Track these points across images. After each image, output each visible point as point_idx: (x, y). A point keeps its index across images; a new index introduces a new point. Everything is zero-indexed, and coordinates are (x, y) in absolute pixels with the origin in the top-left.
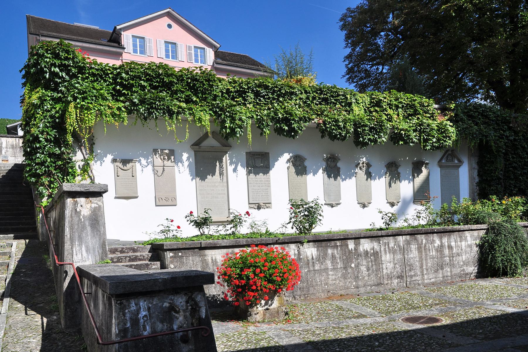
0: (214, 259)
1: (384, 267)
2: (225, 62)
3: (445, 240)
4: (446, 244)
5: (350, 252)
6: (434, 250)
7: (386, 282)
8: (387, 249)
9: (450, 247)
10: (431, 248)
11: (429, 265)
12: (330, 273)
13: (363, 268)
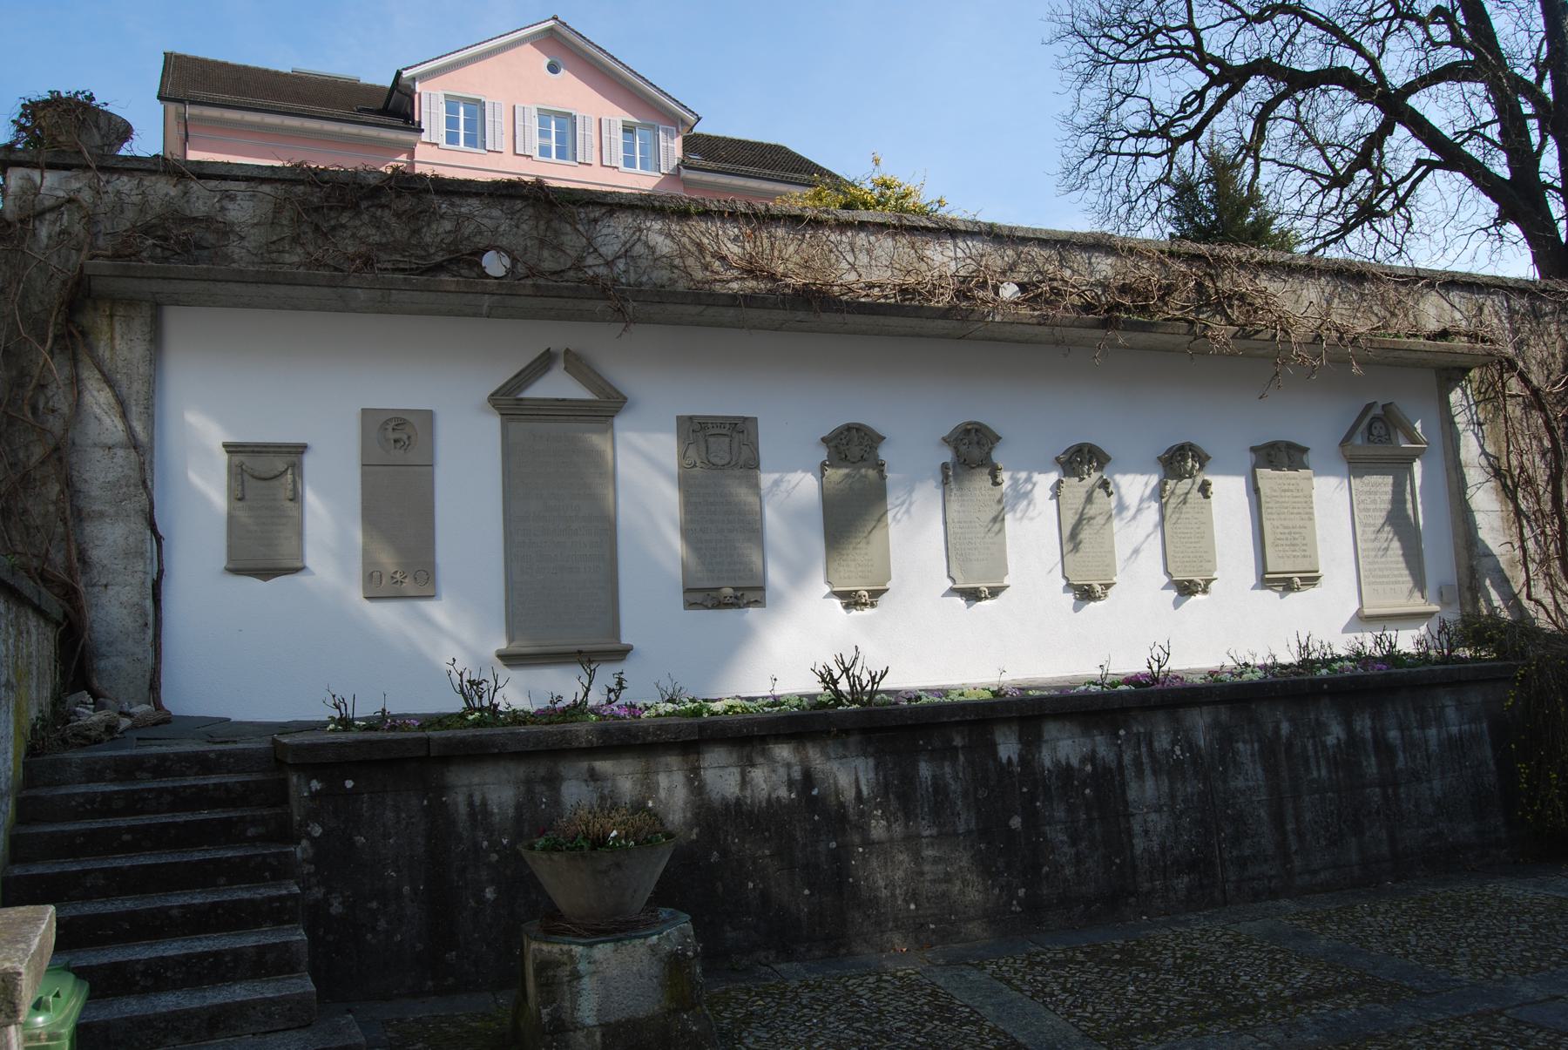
0: (477, 800)
1: (1137, 828)
2: (712, 165)
3: (1364, 724)
4: (1368, 735)
5: (1004, 769)
6: (1322, 763)
7: (1147, 886)
8: (1145, 759)
9: (1384, 749)
10: (1311, 753)
11: (1308, 816)
12: (929, 853)
13: (1057, 834)
